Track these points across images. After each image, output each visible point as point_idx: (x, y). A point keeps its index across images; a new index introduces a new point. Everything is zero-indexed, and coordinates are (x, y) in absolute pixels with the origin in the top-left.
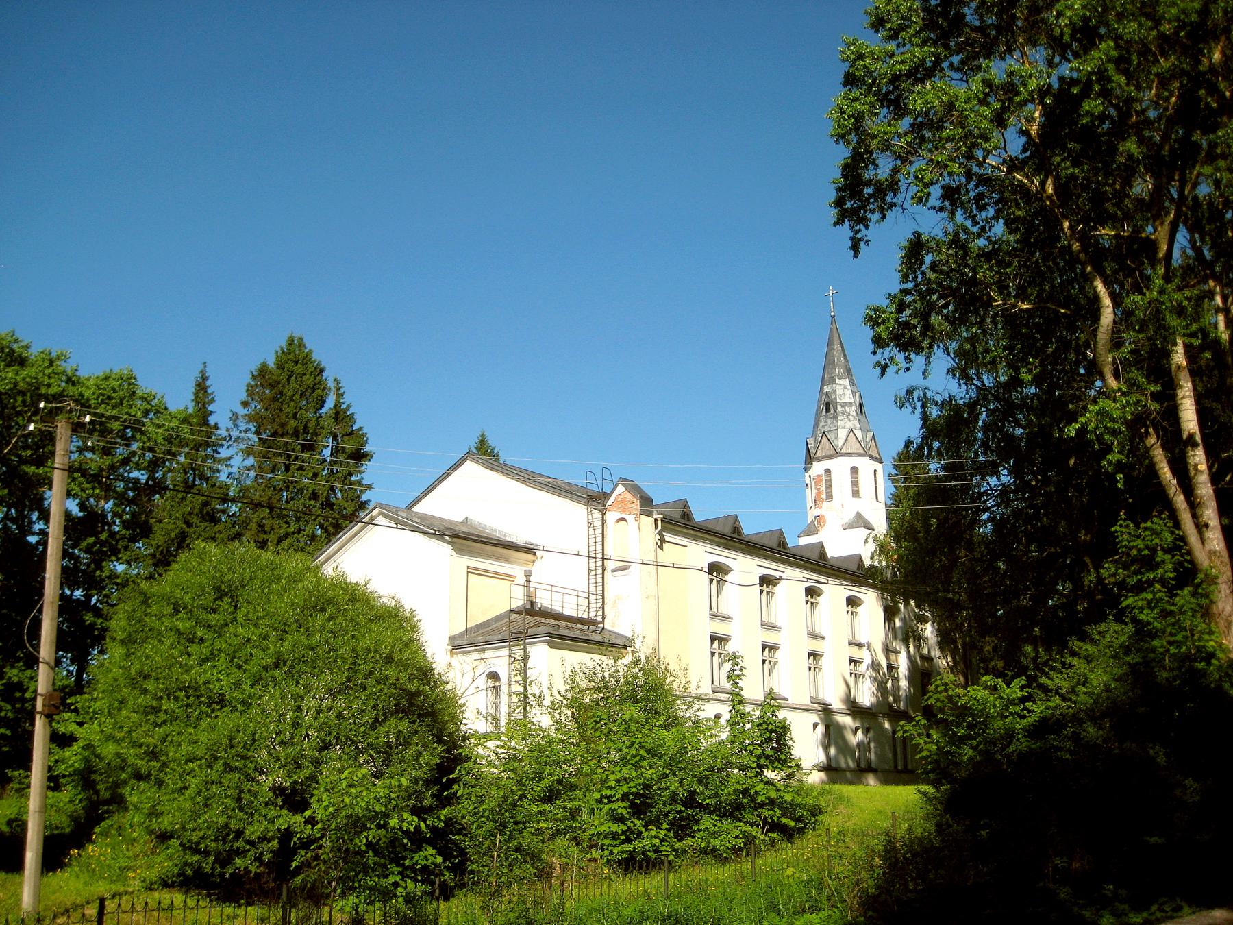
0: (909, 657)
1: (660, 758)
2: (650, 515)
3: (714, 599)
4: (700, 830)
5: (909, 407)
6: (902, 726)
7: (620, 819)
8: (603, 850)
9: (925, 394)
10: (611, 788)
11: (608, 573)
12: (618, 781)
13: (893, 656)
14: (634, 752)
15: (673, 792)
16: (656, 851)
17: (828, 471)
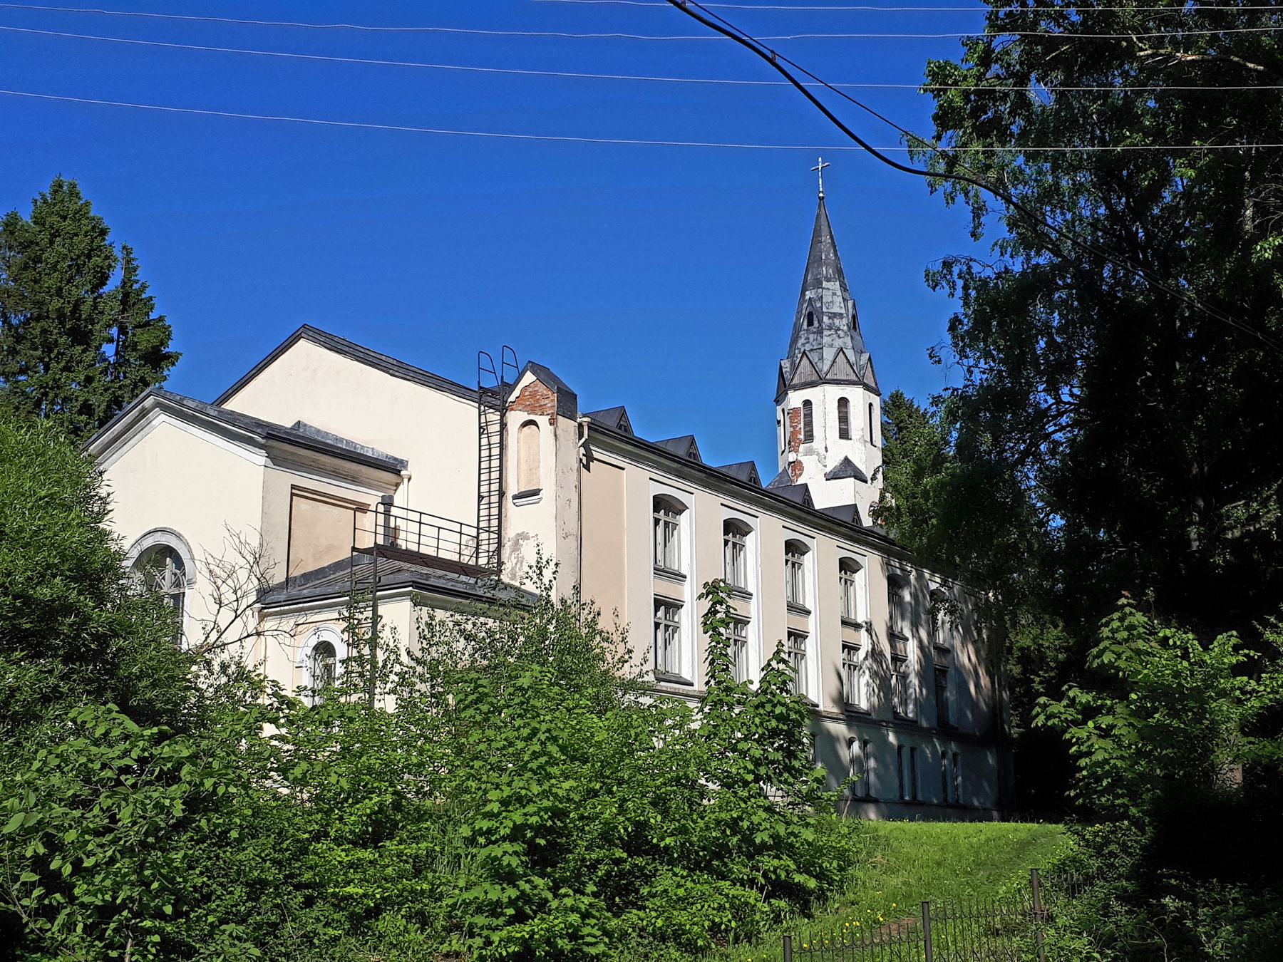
0: (921, 646)
1: (585, 763)
2: (573, 418)
3: (660, 549)
4: (654, 896)
5: (947, 287)
6: (1045, 706)
7: (510, 878)
8: (472, 936)
9: (969, 268)
10: (490, 816)
11: (508, 502)
12: (505, 803)
13: (900, 645)
14: (537, 748)
15: (606, 823)
16: (574, 937)
17: (807, 403)
